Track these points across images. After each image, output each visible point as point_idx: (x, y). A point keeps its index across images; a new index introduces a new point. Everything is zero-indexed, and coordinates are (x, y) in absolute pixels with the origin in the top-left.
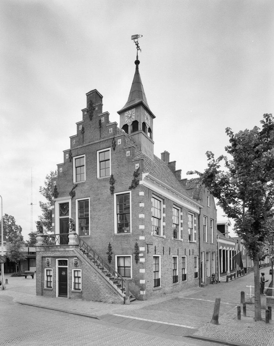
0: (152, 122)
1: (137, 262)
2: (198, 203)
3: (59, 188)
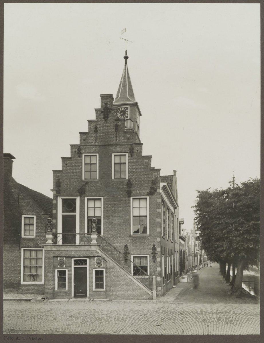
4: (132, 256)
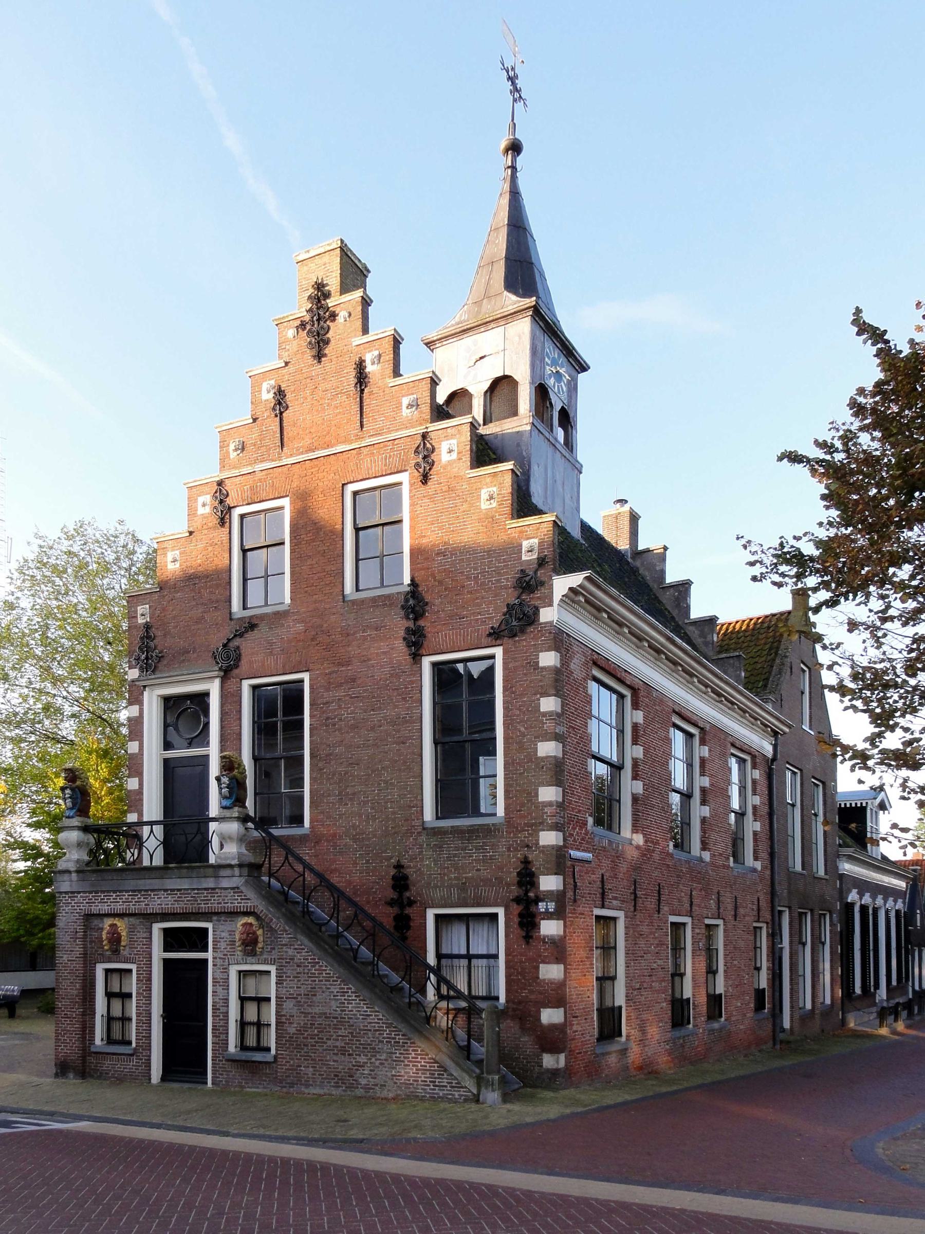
0: (573, 388)
1: (528, 938)
2: (767, 712)
3: (165, 635)
4: (431, 914)
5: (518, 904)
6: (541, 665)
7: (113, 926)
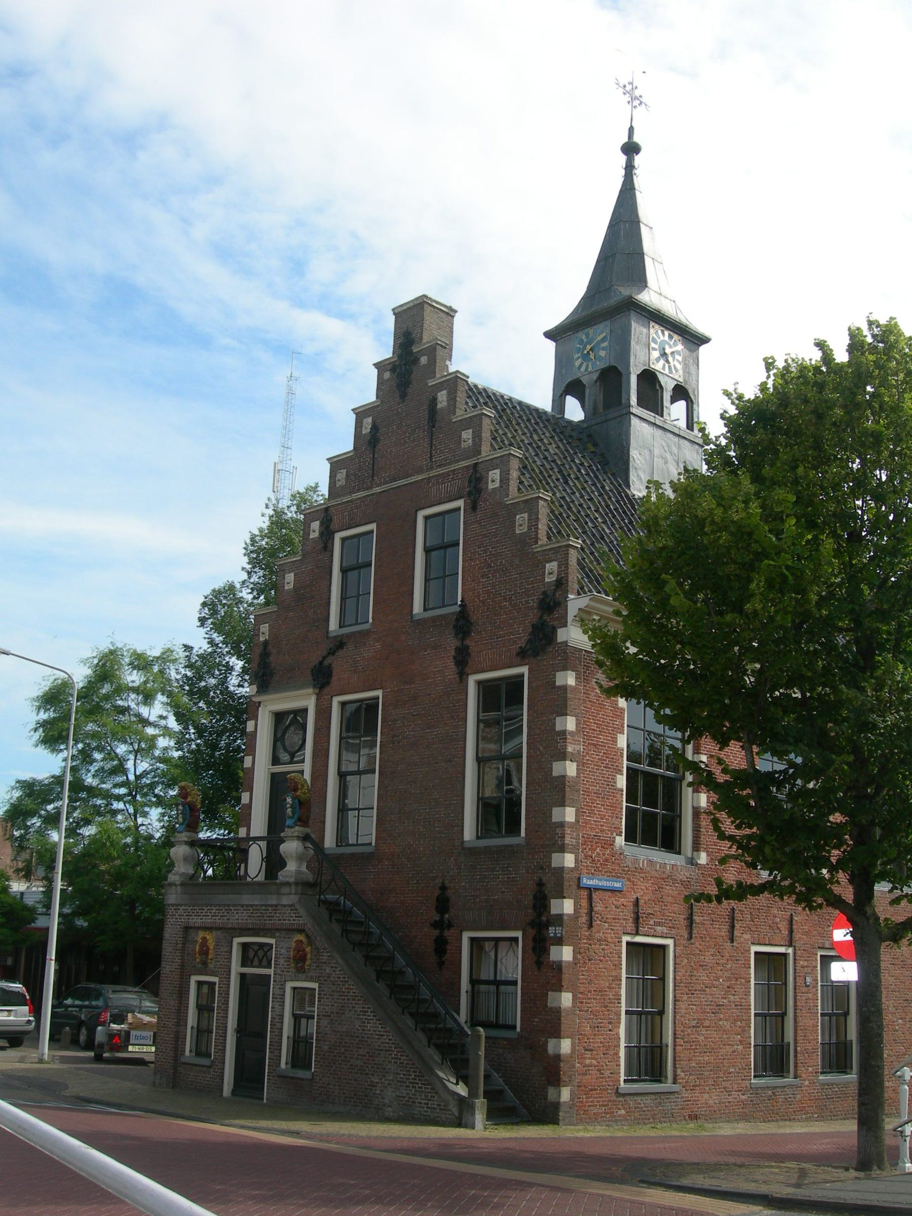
4: (466, 936)
5: (533, 927)
6: (557, 684)
7: (204, 939)
